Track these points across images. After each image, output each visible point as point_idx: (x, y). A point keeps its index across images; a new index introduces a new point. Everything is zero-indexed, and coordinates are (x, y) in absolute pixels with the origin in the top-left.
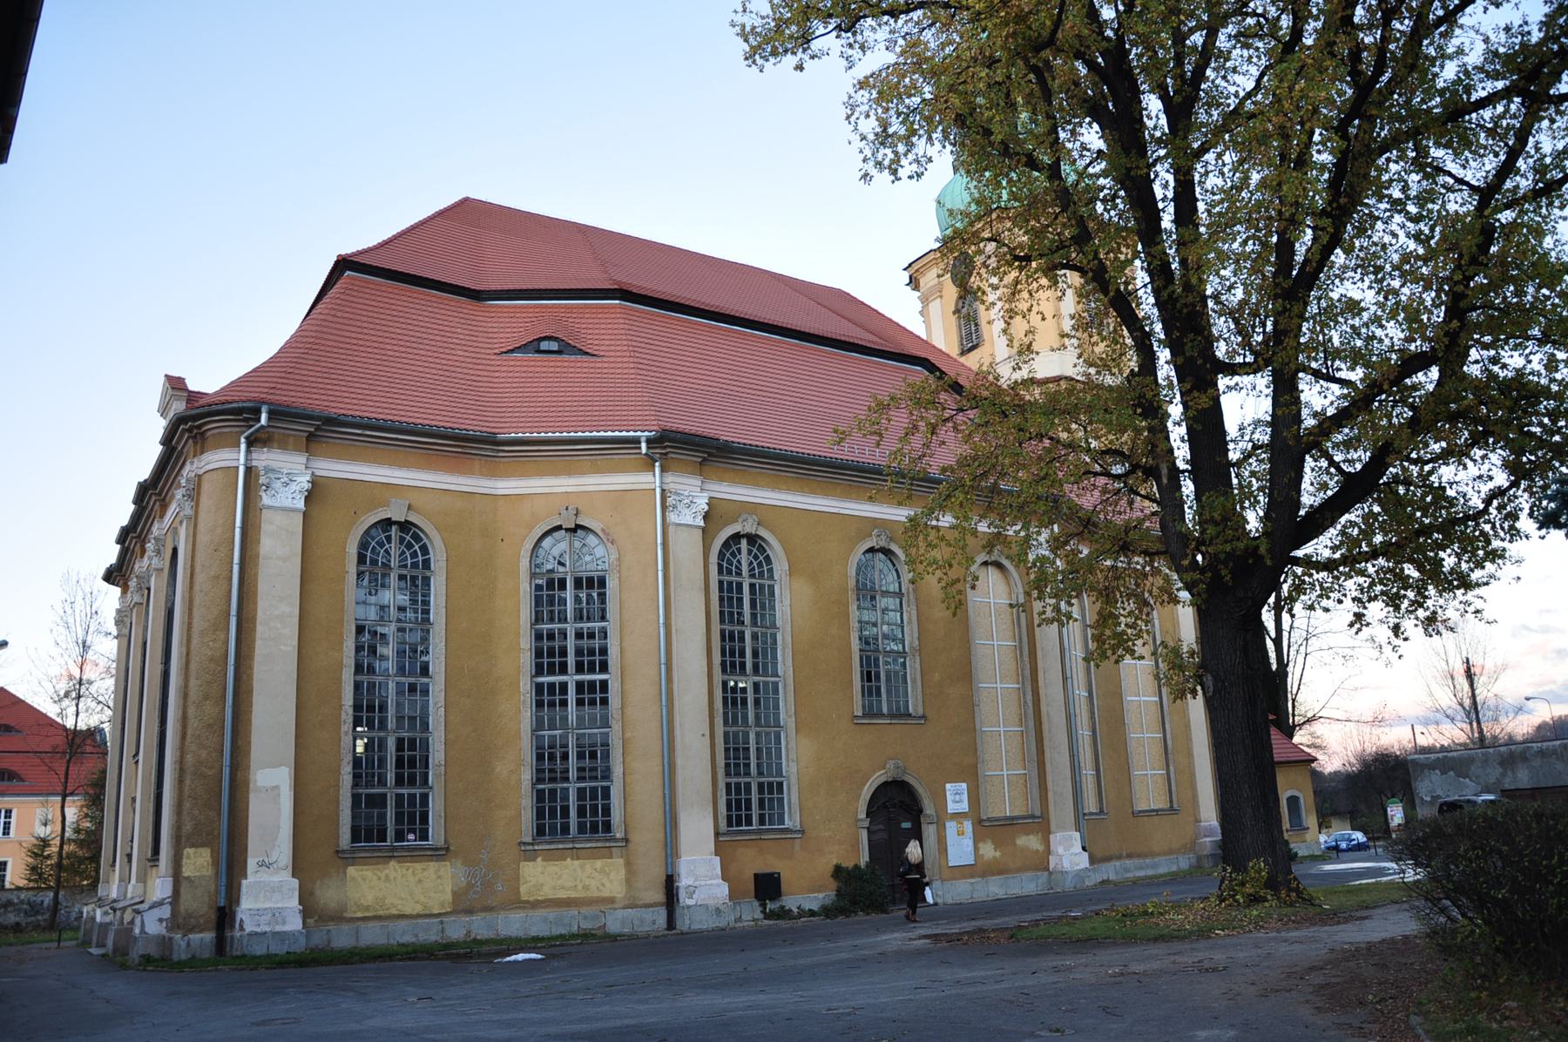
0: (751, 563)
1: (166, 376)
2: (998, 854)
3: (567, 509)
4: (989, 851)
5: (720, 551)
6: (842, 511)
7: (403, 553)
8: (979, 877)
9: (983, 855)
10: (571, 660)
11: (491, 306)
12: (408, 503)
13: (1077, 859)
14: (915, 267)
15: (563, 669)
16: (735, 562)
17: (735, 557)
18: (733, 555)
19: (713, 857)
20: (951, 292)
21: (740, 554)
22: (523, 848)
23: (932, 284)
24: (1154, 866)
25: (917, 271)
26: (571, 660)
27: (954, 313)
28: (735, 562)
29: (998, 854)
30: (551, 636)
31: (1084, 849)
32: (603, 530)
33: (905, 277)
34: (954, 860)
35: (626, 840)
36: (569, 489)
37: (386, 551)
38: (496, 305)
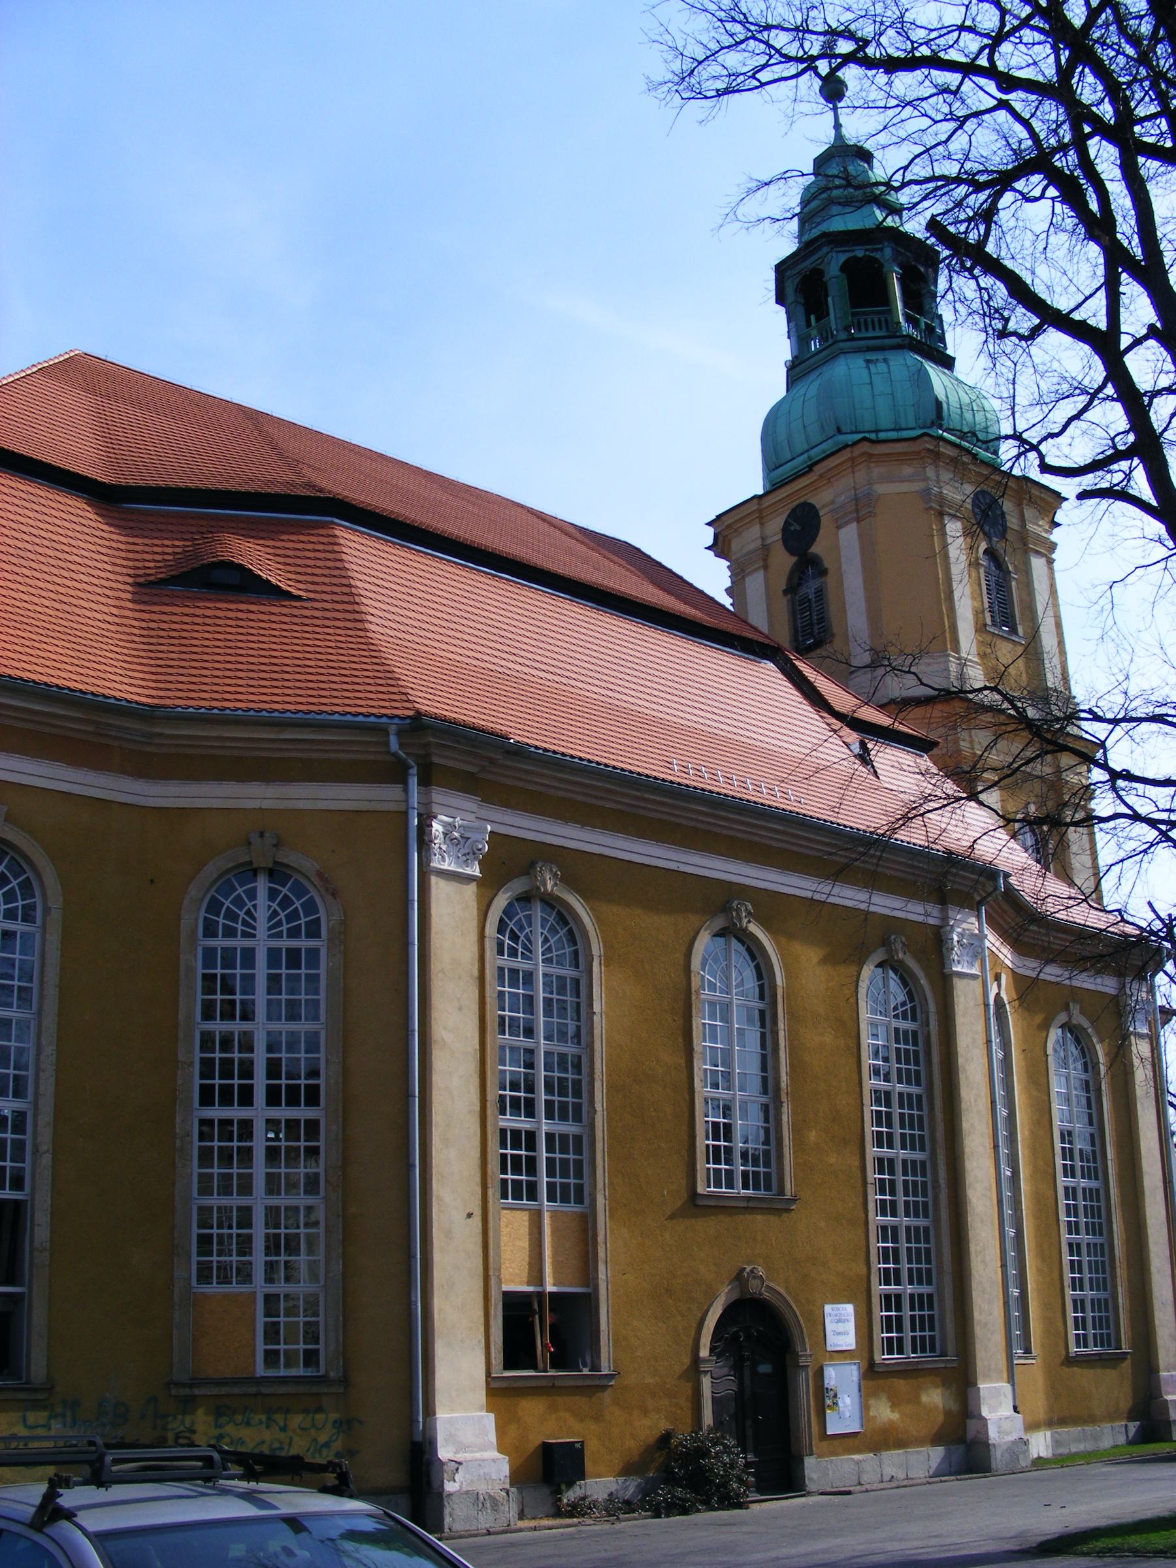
0: (275, 913)
1: (708, 548)
2: (895, 1416)
3: (262, 835)
4: (884, 1412)
5: (501, 920)
6: (683, 868)
7: (275, 913)
8: (870, 1451)
9: (874, 1418)
10: (260, 1083)
11: (133, 511)
12: (5, 809)
13: (1006, 1426)
14: (727, 521)
15: (246, 1097)
16: (242, 914)
17: (522, 928)
18: (239, 902)
19: (484, 1413)
20: (783, 561)
21: (530, 925)
22: (173, 1392)
23: (752, 546)
24: (496, 1316)
25: (729, 526)
26: (260, 1083)
27: (785, 592)
28: (242, 914)
29: (895, 1416)
30: (226, 1043)
31: (1015, 1409)
32: (320, 875)
33: (708, 535)
34: (834, 1427)
35: (345, 1381)
36: (266, 804)
37: (248, 913)
38: (138, 510)
